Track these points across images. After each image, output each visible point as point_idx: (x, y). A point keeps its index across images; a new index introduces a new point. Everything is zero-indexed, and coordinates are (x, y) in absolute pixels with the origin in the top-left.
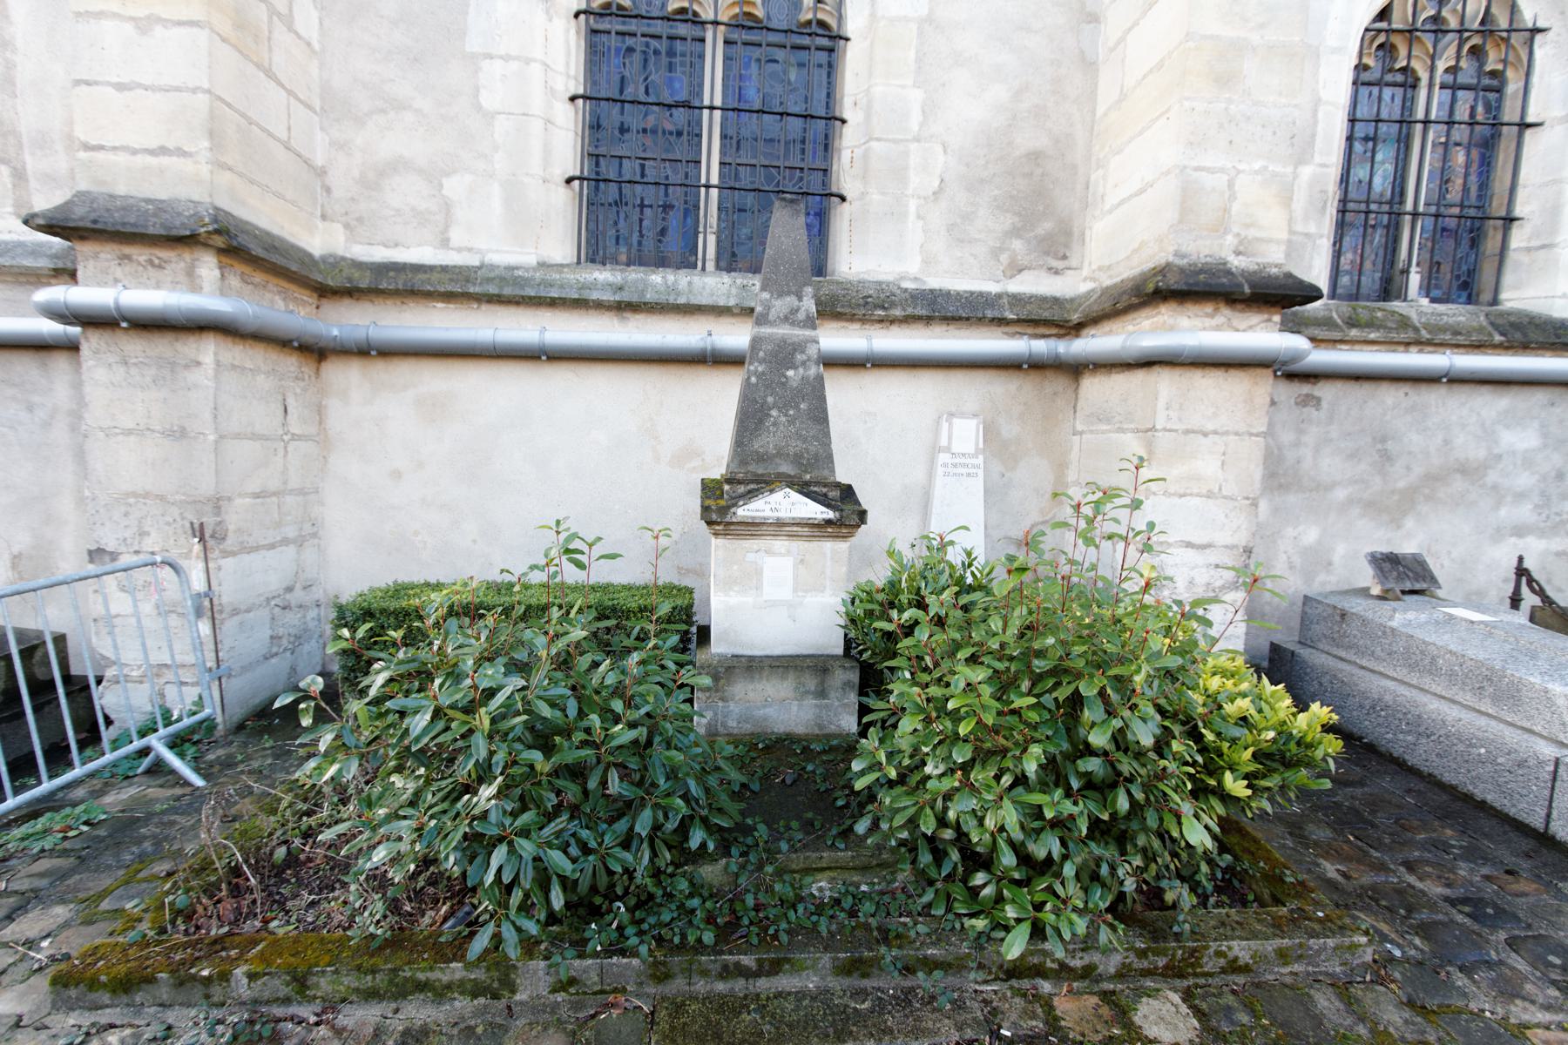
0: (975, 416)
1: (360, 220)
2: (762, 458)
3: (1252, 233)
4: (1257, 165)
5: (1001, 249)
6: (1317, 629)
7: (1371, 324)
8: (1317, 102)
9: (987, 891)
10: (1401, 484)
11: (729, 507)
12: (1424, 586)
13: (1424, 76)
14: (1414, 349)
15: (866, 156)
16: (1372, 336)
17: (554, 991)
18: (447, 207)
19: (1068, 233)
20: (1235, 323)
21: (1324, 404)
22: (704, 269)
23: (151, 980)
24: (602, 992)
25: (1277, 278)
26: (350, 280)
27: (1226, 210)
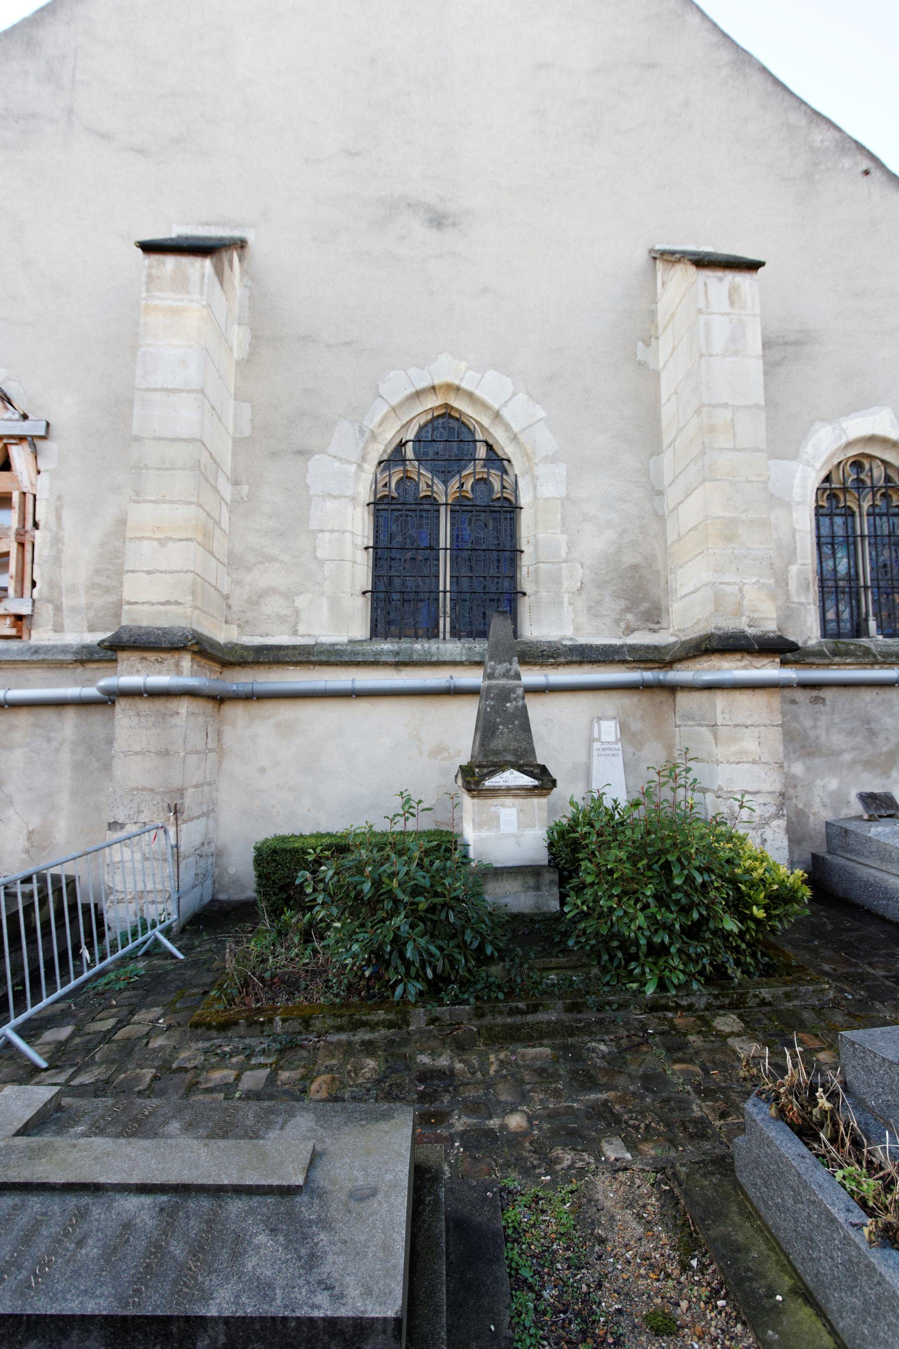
0: (614, 718)
1: (247, 622)
2: (496, 753)
3: (756, 615)
4: (754, 580)
5: (620, 620)
6: (835, 841)
7: (847, 654)
8: (794, 532)
9: (636, 971)
10: (885, 749)
11: (480, 781)
12: (893, 812)
13: (856, 510)
14: (877, 667)
15: (537, 571)
16: (848, 661)
17: (428, 1025)
18: (297, 612)
19: (659, 609)
20: (754, 664)
21: (828, 701)
22: (444, 638)
23: (236, 1023)
24: (451, 1024)
25: (773, 639)
26: (242, 657)
27: (740, 604)
